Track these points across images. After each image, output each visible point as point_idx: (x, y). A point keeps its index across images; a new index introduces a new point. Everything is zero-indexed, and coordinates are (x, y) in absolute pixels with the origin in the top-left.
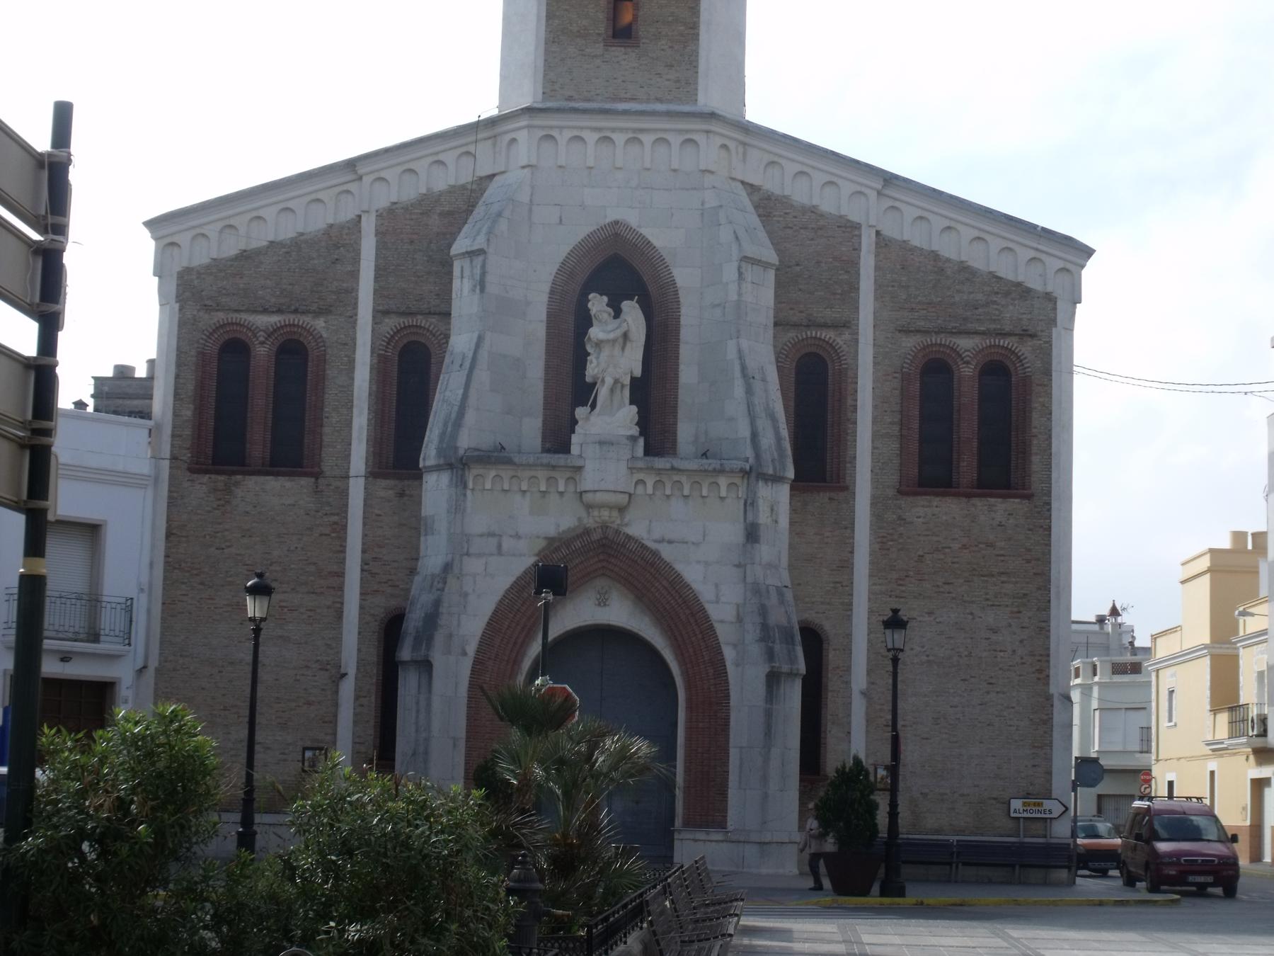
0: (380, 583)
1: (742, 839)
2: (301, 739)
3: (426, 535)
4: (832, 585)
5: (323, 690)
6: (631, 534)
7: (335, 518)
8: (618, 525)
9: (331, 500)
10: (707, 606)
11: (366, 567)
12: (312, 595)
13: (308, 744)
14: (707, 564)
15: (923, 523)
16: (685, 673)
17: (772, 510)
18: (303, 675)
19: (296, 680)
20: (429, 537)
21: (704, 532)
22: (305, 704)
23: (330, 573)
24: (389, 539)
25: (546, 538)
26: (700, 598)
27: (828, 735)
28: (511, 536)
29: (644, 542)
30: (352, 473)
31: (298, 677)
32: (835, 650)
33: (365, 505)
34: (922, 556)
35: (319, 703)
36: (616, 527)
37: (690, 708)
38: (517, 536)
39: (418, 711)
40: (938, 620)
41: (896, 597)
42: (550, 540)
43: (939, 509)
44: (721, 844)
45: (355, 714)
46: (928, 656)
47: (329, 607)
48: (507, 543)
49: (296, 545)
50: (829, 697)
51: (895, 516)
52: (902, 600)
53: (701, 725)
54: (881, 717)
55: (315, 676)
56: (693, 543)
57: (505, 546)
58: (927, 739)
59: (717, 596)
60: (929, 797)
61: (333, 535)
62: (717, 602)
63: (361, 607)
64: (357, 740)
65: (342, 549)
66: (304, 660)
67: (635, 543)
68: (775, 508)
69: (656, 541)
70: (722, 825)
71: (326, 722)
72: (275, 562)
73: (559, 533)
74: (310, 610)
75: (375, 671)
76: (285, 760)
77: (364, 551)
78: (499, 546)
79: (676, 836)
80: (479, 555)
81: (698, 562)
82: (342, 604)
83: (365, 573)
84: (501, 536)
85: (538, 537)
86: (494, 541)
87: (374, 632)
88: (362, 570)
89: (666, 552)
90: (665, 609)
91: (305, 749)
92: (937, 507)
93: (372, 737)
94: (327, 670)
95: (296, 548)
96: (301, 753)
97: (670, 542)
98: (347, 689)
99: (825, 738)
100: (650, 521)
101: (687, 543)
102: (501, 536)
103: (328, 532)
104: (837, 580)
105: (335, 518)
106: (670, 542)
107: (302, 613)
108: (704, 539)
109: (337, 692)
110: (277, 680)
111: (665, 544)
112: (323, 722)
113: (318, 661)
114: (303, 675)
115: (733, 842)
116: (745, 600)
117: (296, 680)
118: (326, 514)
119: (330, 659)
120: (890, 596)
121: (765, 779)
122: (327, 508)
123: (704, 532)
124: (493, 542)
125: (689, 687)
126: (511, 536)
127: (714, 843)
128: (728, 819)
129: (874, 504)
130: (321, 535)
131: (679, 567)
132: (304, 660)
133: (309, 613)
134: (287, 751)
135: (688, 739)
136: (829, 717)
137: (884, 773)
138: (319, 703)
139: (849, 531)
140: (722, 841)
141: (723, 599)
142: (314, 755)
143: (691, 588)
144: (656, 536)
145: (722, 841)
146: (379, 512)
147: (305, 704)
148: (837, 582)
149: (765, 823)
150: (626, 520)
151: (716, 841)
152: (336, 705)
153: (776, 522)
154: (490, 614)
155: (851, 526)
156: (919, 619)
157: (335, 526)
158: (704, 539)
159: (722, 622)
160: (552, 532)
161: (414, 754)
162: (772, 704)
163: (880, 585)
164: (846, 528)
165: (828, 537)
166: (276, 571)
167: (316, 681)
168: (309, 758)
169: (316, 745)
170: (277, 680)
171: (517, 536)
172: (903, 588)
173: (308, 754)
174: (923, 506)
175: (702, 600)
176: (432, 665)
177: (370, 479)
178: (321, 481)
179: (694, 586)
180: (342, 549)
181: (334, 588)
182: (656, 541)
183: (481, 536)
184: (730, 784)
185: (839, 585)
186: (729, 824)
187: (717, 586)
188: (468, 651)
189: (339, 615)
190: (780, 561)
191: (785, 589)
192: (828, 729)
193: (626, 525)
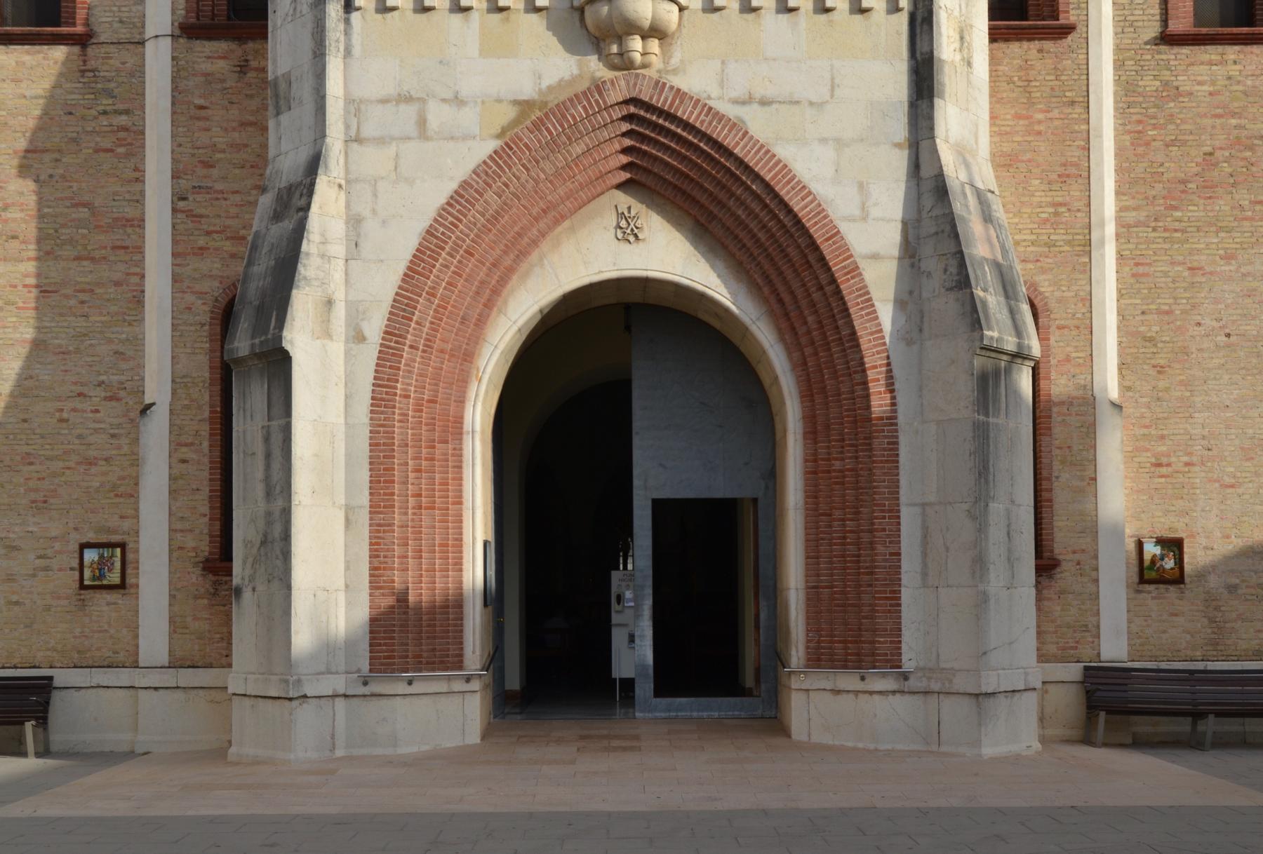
0: (208, 233)
1: (935, 686)
2: (76, 529)
3: (278, 114)
4: (1051, 210)
5: (113, 436)
6: (684, 87)
7: (123, 120)
8: (659, 71)
9: (112, 85)
10: (844, 227)
11: (181, 204)
12: (85, 263)
13: (91, 537)
14: (840, 143)
15: (1211, 94)
16: (801, 367)
17: (962, 38)
18: (74, 410)
19: (61, 420)
20: (284, 118)
21: (833, 79)
22: (79, 463)
23: (116, 220)
24: (223, 151)
25: (516, 103)
26: (830, 212)
27: (1055, 484)
28: (444, 100)
29: (711, 103)
30: (150, 32)
31: (65, 415)
32: (1059, 328)
33: (175, 89)
34: (1211, 154)
35: (106, 460)
36: (655, 76)
37: (812, 432)
38: (458, 101)
39: (268, 456)
40: (1243, 270)
41: (1166, 230)
42: (525, 106)
43: (1238, 67)
44: (891, 697)
45: (172, 478)
46: (1228, 335)
47: (117, 284)
48: (438, 115)
49: (50, 171)
50: (1054, 415)
51: (1158, 83)
52: (1178, 235)
53: (837, 465)
54: (1147, 450)
55: (97, 411)
56: (811, 104)
57: (433, 122)
58: (1232, 486)
59: (863, 207)
60: (1240, 592)
61: (121, 150)
62: (865, 218)
63: (176, 279)
64: (179, 526)
65: (137, 174)
66: (75, 383)
67: (694, 107)
68: (967, 38)
69: (736, 102)
70: (893, 661)
71: (121, 496)
72: (13, 204)
73: (540, 92)
74: (83, 291)
75: (207, 398)
76: (46, 569)
77: (176, 176)
78: (422, 122)
79: (795, 683)
80: (381, 141)
81: (823, 141)
82: (143, 276)
83: (179, 216)
84: (422, 101)
85: (499, 101)
86: (409, 111)
87: (203, 325)
88: (174, 210)
89: (759, 124)
90: (758, 240)
91: (83, 547)
92: (1235, 62)
93: (206, 519)
94: (118, 400)
95: (51, 176)
96: (77, 555)
97: (764, 103)
98: (156, 431)
99: (1050, 490)
100: (723, 62)
101: (797, 102)
102: (422, 101)
103: (109, 146)
104: (1060, 199)
105: (123, 120)
106: (764, 103)
107: (67, 297)
108: (832, 96)
109: (136, 441)
110: (25, 421)
111: (755, 106)
112: (117, 495)
113: (100, 384)
114: (74, 410)
115: (914, 693)
116: (919, 211)
117: (61, 420)
118: (105, 113)
119: (123, 378)
120: (1154, 229)
121: (979, 564)
122: (105, 102)
123: (833, 79)
124: (408, 112)
125: (809, 392)
126: (444, 100)
127: (876, 697)
128: (904, 647)
129: (1119, 65)
130: (97, 151)
131: (784, 152)
132: (75, 383)
133: (82, 296)
134: (49, 552)
135: (812, 495)
136: (1056, 452)
137: (1157, 550)
138: (106, 460)
139: (1078, 109)
140: (894, 692)
141: (875, 212)
142: (101, 556)
143: (810, 193)
144: (738, 91)
145: (894, 692)
146: (201, 102)
147: (79, 463)
148: (1061, 204)
149: (985, 653)
150: (675, 61)
151: (880, 693)
152: (135, 461)
153: (969, 64)
154: (409, 257)
155: (1085, 102)
156: (1208, 269)
157: (122, 135)
158: (832, 96)
159: (875, 257)
160: (528, 90)
161: (263, 543)
162: (987, 415)
163: (1134, 209)
164: (1073, 103)
165: (1040, 122)
166: (14, 220)
167: (99, 422)
168: (92, 563)
169: (103, 538)
170: (25, 421)
171: (458, 101)
172: (1178, 214)
173: (90, 556)
174: (1211, 63)
175: (832, 215)
176: (290, 358)
177: (181, 40)
178: (91, 51)
179: (815, 187)
180: (137, 174)
181: (126, 248)
182: (736, 102)
183: (384, 101)
184: (905, 579)
185: (1063, 209)
186: (904, 658)
187: (861, 186)
188: (367, 333)
189: (138, 300)
190: (976, 143)
191: (989, 195)
192: (1055, 474)
193: (675, 71)
